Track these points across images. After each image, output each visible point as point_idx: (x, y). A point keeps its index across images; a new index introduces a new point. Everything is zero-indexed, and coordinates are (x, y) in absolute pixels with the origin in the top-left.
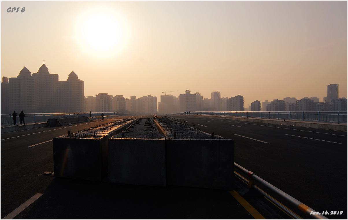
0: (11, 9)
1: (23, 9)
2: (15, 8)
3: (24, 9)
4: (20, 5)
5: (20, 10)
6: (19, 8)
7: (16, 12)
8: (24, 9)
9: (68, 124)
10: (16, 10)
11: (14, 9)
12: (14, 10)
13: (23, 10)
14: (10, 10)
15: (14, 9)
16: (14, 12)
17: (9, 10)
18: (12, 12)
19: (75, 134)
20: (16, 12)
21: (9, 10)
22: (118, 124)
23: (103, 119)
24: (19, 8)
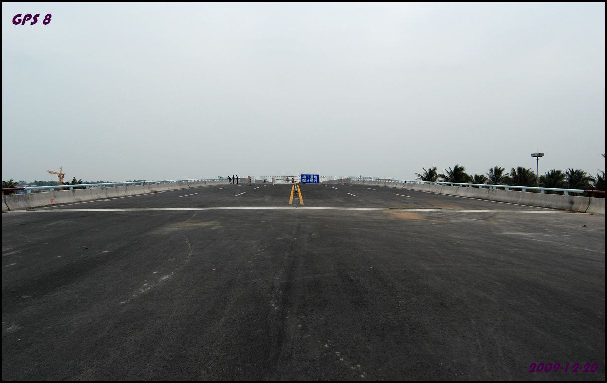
0: (22, 18)
1: (46, 18)
2: (30, 16)
3: (47, 21)
4: (42, 9)
5: (40, 19)
6: (38, 15)
7: (32, 23)
8: (48, 17)
9: (233, 196)
10: (32, 20)
11: (28, 17)
12: (28, 19)
13: (48, 18)
14: (20, 20)
15: (28, 17)
16: (28, 23)
17: (16, 20)
18: (23, 23)
19: (595, 371)
20: (32, 23)
21: (16, 20)
22: (578, 246)
23: (288, 179)
24: (38, 15)
